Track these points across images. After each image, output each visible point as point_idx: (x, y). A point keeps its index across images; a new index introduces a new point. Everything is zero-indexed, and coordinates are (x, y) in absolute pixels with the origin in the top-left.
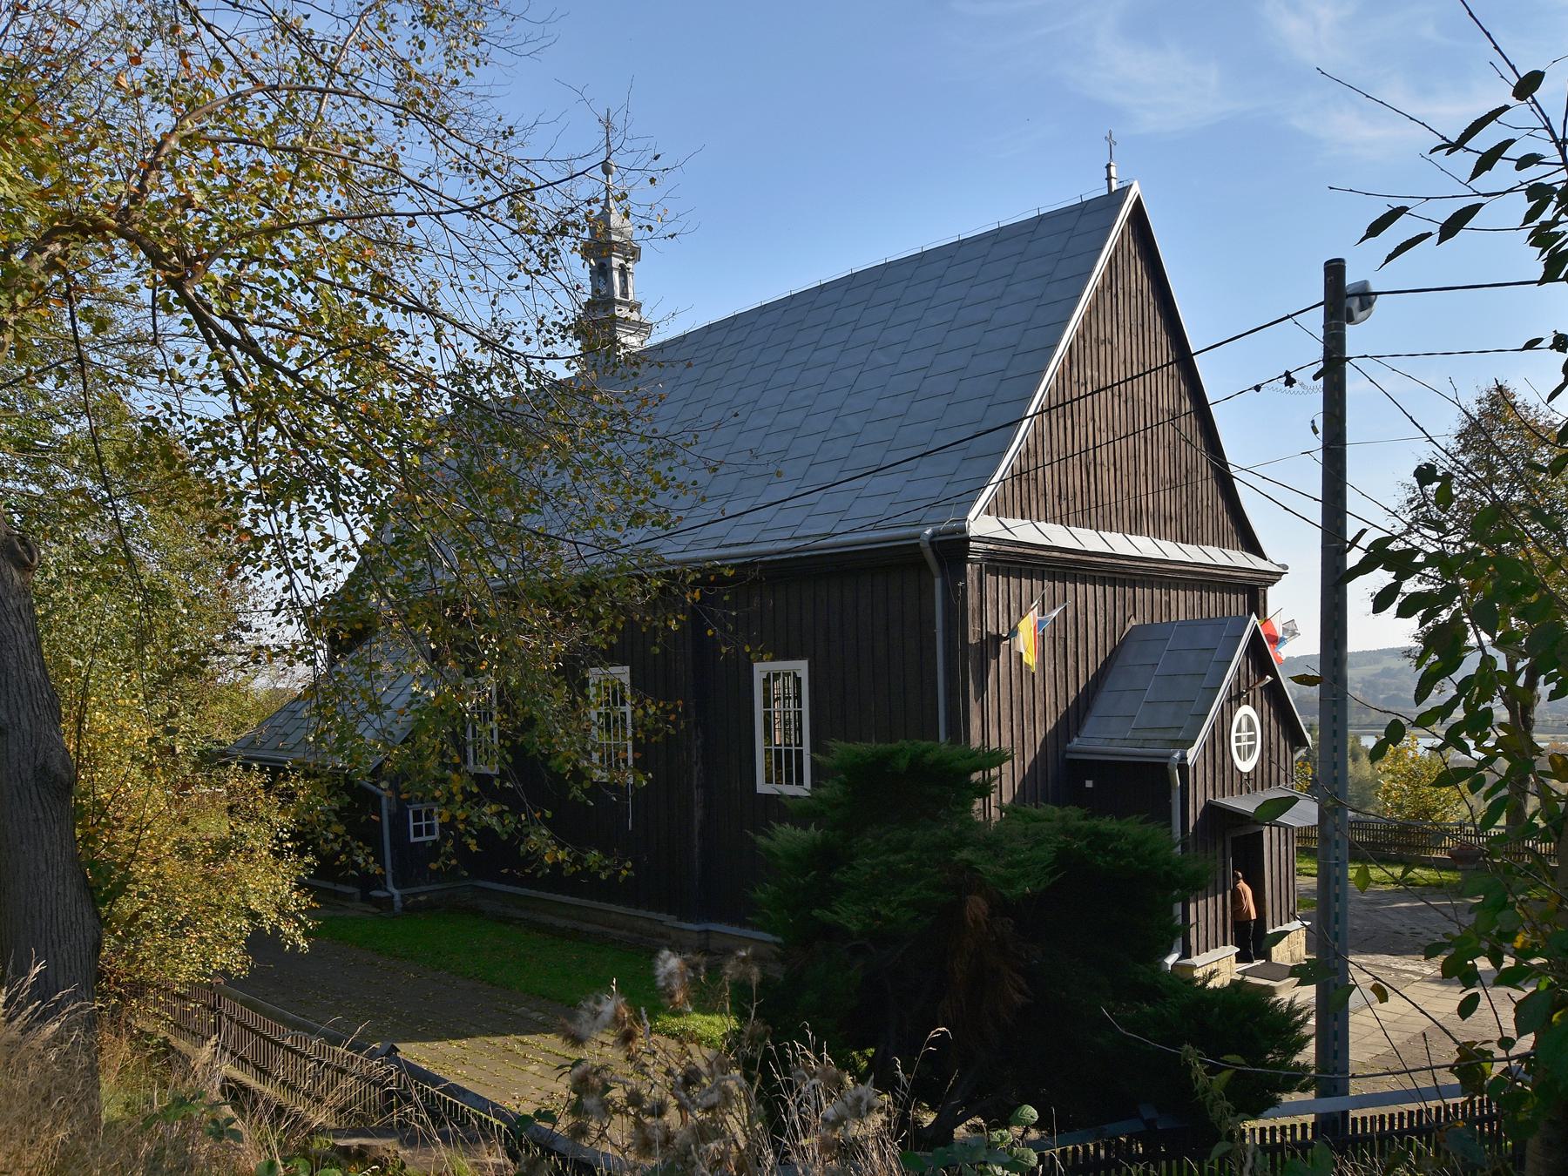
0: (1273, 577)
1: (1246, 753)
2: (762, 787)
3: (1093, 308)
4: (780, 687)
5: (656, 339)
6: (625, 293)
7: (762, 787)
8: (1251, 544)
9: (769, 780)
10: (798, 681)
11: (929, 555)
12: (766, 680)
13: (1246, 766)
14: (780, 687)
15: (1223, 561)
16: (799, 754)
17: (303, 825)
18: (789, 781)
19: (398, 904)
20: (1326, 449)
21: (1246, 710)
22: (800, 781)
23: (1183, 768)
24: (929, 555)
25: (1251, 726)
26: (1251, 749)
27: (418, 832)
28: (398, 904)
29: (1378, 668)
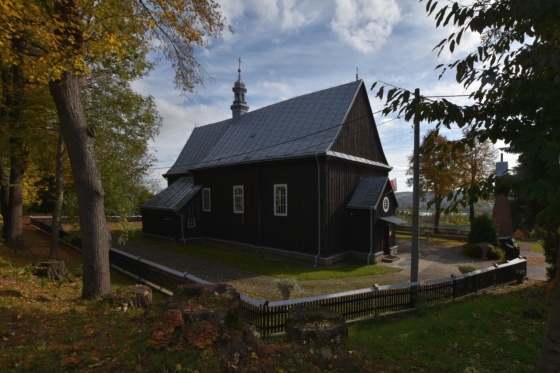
0: (390, 170)
1: (386, 208)
2: (275, 214)
3: (353, 106)
4: (280, 191)
5: (249, 111)
6: (243, 100)
7: (275, 214)
8: (386, 163)
9: (277, 212)
10: (285, 189)
11: (317, 159)
12: (277, 189)
13: (386, 211)
14: (280, 191)
15: (380, 165)
16: (285, 206)
17: (68, 62)
18: (282, 212)
19: (185, 243)
20: (415, 132)
21: (386, 198)
22: (285, 213)
23: (373, 210)
24: (317, 159)
25: (387, 202)
26: (387, 207)
27: (190, 225)
28: (185, 243)
29: (401, 196)
